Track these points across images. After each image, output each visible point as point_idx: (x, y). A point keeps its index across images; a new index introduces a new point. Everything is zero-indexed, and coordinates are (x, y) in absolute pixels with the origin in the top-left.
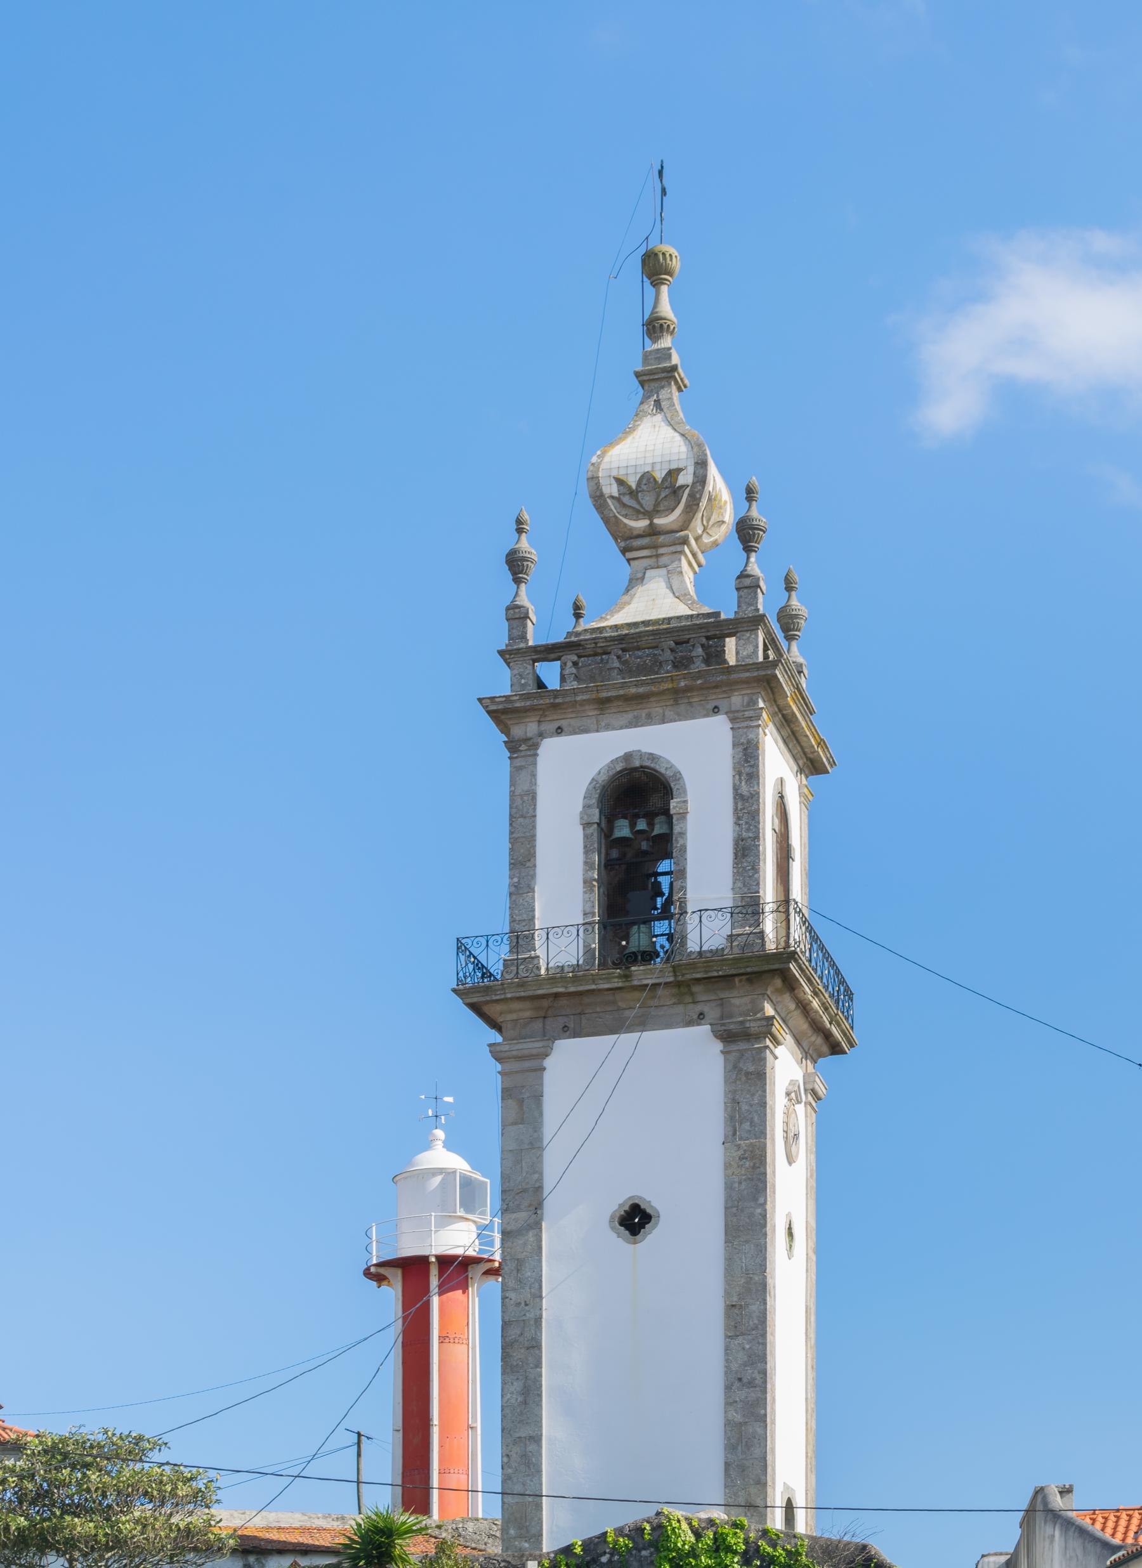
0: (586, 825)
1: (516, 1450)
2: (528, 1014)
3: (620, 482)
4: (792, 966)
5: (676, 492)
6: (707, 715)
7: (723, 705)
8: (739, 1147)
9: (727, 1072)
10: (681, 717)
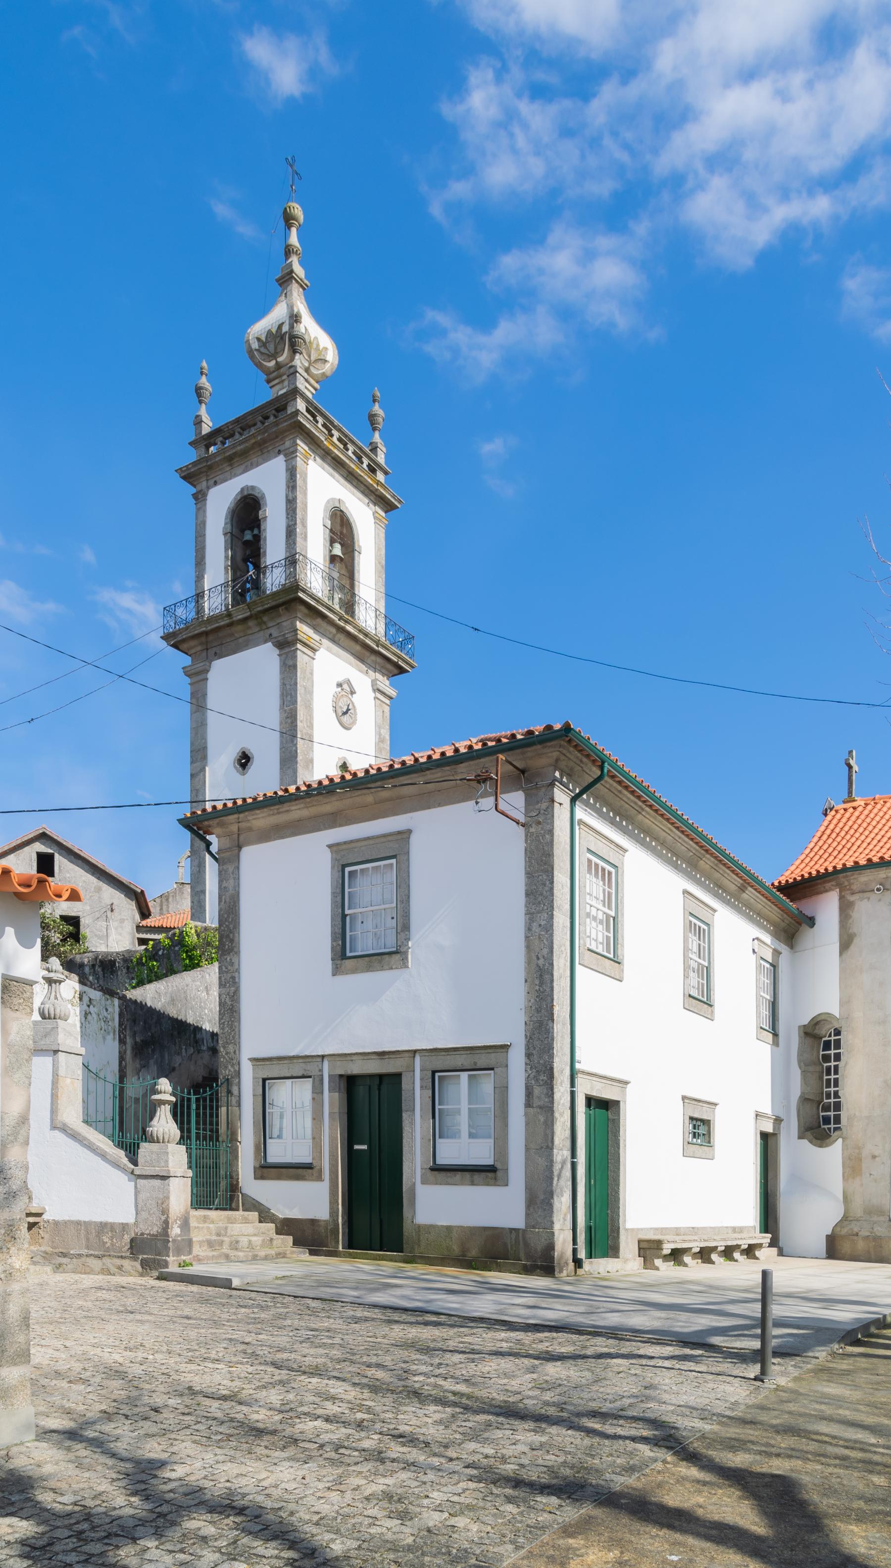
0: (225, 534)
1: (196, 898)
2: (199, 648)
3: (258, 339)
4: (301, 595)
5: (282, 337)
6: (276, 457)
7: (282, 448)
8: (285, 711)
9: (281, 667)
10: (265, 460)
